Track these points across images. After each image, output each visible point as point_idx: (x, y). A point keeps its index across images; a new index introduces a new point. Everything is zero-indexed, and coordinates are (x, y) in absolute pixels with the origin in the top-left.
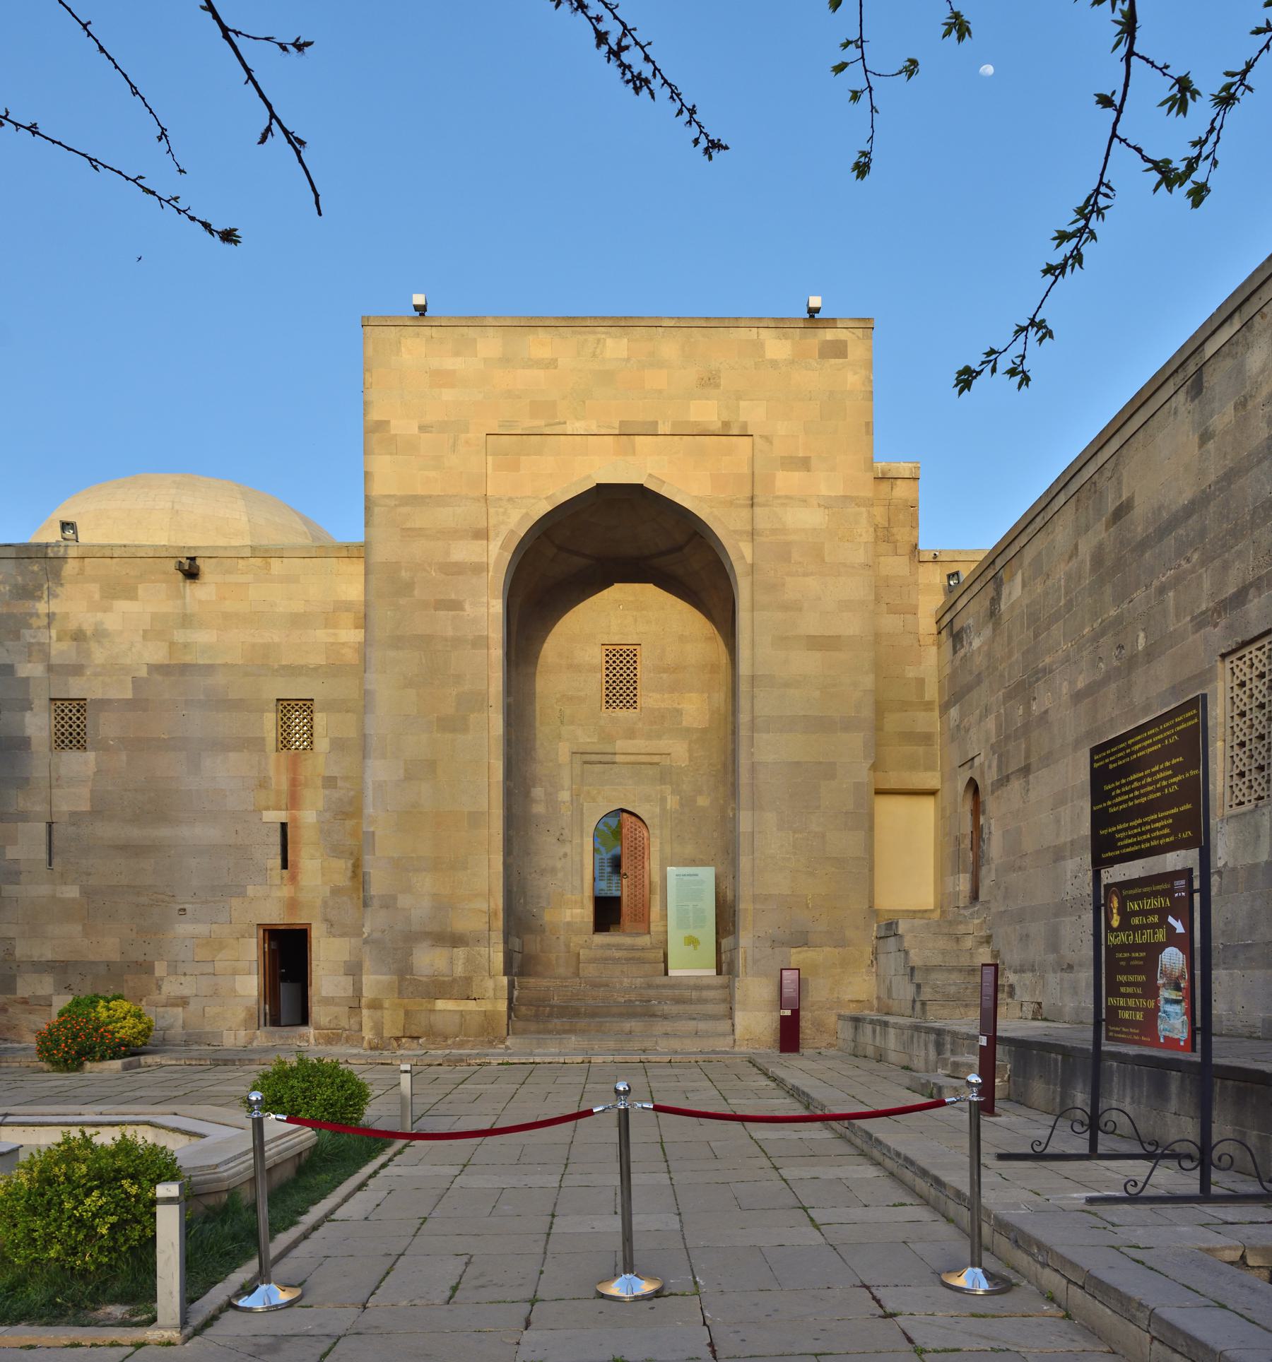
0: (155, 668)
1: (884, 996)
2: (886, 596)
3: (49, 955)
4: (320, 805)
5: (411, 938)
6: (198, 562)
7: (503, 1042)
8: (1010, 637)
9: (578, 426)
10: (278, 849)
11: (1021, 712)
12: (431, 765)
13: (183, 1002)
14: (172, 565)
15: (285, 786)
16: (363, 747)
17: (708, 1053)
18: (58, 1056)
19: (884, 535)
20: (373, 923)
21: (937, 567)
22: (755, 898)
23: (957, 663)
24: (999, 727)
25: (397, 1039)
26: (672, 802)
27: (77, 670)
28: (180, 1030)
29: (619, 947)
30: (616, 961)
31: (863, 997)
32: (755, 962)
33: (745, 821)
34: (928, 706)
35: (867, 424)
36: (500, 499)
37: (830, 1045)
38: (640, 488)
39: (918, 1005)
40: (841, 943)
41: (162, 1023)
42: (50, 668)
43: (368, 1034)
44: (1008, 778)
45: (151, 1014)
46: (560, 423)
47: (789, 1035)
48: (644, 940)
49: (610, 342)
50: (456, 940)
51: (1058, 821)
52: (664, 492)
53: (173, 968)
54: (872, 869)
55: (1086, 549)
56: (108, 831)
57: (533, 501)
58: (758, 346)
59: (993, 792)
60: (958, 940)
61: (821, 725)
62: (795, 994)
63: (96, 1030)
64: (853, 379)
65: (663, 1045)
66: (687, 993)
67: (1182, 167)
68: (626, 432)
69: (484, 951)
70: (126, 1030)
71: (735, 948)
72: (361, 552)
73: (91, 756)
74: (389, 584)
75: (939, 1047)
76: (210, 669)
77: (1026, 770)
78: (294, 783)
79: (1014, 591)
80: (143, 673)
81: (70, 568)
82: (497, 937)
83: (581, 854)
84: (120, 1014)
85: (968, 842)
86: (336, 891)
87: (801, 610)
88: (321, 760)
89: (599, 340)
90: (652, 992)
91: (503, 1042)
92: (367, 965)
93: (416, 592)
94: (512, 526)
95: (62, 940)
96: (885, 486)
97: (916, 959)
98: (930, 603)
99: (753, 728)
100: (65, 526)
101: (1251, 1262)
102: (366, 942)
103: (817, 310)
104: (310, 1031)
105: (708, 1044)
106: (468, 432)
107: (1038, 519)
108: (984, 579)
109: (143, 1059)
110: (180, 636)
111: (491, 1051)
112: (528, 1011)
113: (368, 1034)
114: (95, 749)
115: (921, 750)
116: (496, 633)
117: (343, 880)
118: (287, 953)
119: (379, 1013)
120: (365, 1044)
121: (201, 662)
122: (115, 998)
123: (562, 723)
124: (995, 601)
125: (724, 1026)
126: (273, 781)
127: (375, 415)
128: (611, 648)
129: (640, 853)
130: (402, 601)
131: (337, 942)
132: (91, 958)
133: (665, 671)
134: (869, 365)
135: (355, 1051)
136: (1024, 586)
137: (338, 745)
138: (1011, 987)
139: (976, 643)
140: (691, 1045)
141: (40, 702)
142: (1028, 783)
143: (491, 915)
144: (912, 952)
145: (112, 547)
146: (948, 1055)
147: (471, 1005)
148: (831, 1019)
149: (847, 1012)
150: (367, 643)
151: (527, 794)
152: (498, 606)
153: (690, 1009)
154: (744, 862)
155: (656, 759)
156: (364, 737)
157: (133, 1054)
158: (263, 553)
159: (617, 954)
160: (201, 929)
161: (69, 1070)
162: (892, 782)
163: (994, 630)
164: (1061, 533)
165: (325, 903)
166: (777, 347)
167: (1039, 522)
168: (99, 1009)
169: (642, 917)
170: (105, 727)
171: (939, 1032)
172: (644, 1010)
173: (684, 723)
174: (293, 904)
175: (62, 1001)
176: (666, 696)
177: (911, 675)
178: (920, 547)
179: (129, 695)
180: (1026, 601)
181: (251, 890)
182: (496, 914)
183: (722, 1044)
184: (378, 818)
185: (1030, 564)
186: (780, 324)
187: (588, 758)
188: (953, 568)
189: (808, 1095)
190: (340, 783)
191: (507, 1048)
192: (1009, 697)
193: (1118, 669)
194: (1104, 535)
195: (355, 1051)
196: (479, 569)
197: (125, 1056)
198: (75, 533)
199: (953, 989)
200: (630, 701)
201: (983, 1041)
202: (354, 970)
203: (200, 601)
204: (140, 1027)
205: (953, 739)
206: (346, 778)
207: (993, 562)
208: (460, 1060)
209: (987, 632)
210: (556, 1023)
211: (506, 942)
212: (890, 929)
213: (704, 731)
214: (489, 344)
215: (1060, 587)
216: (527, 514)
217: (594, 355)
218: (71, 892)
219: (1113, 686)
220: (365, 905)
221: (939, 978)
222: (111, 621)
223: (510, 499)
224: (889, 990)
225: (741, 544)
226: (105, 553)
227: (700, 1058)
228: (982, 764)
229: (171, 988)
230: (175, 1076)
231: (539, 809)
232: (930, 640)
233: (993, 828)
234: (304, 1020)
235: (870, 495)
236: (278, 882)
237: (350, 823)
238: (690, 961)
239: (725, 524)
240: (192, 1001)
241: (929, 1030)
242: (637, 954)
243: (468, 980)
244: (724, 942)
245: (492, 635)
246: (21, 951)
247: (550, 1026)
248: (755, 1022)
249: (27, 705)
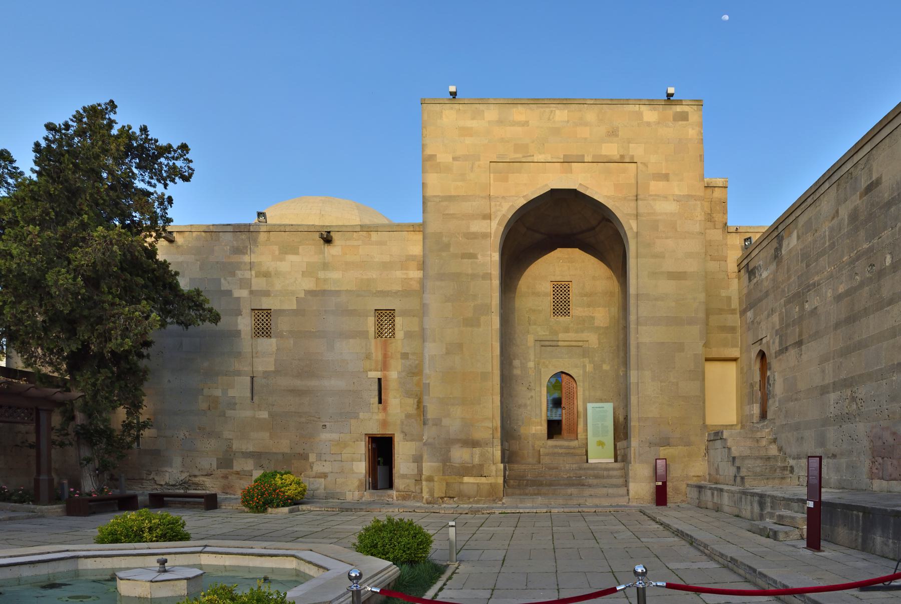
0: (309, 292)
1: (713, 472)
2: (712, 253)
3: (251, 449)
4: (399, 368)
5: (450, 442)
6: (332, 234)
7: (501, 500)
8: (788, 270)
9: (541, 158)
10: (376, 393)
11: (797, 310)
12: (460, 346)
13: (324, 476)
14: (317, 235)
15: (380, 357)
16: (422, 335)
17: (614, 507)
18: (253, 504)
19: (709, 218)
20: (429, 434)
21: (737, 235)
22: (639, 419)
23: (752, 286)
24: (781, 320)
25: (442, 498)
26: (589, 368)
27: (267, 294)
28: (323, 491)
29: (561, 447)
30: (560, 454)
31: (701, 474)
32: (640, 455)
33: (633, 376)
34: (733, 312)
35: (701, 156)
37: (683, 501)
38: (574, 191)
39: (738, 479)
40: (688, 444)
41: (312, 487)
42: (251, 292)
43: (426, 495)
44: (787, 349)
45: (307, 483)
47: (661, 496)
48: (575, 443)
49: (558, 112)
50: (475, 444)
51: (823, 371)
52: (588, 193)
53: (319, 457)
54: (704, 403)
55: (844, 213)
56: (284, 382)
58: (640, 115)
59: (776, 357)
60: (758, 441)
61: (674, 321)
62: (664, 473)
63: (275, 491)
64: (692, 133)
65: (590, 502)
66: (601, 472)
68: (567, 161)
69: (490, 450)
70: (291, 491)
71: (629, 446)
72: (420, 228)
73: (273, 340)
74: (435, 244)
75: (762, 505)
76: (337, 293)
77: (800, 343)
78: (385, 356)
79: (792, 242)
80: (302, 295)
81: (262, 237)
82: (497, 442)
83: (540, 396)
84: (288, 482)
85: (758, 386)
86: (408, 416)
87: (664, 257)
88: (399, 343)
90: (582, 472)
91: (501, 500)
92: (425, 457)
93: (451, 249)
94: (503, 213)
95: (259, 440)
96: (709, 191)
97: (735, 452)
98: (734, 255)
99: (638, 323)
100: (260, 214)
102: (425, 444)
103: (672, 95)
104: (394, 493)
105: (614, 501)
106: (479, 160)
107: (809, 200)
108: (770, 238)
109: (300, 507)
110: (321, 275)
111: (494, 505)
112: (515, 483)
113: (426, 495)
114: (276, 337)
115: (729, 336)
116: (495, 272)
117: (412, 410)
118: (381, 449)
119: (432, 484)
120: (424, 501)
121: (333, 289)
122: (286, 473)
124: (778, 249)
125: (623, 491)
126: (374, 355)
127: (429, 151)
129: (572, 396)
130: (444, 254)
131: (409, 443)
132: (274, 450)
133: (585, 295)
134: (701, 125)
135: (418, 504)
136: (798, 238)
137: (409, 335)
138: (792, 467)
139: (765, 274)
140: (605, 502)
141: (246, 311)
142: (801, 350)
143: (494, 430)
144: (733, 449)
145: (285, 225)
146: (768, 510)
147: (483, 480)
148: (683, 487)
149: (694, 482)
150: (425, 277)
151: (511, 364)
152: (496, 257)
153: (604, 481)
154: (633, 399)
155: (580, 344)
156: (423, 329)
157: (295, 504)
158: (367, 229)
159: (560, 451)
160: (335, 436)
161: (259, 512)
162: (714, 354)
163: (777, 266)
164: (826, 205)
165: (402, 423)
166: (650, 115)
167: (810, 201)
169: (573, 431)
170: (281, 324)
171: (762, 496)
172: (578, 482)
173: (596, 324)
174: (384, 423)
175: (257, 474)
177: (724, 295)
178: (728, 224)
179: (295, 307)
180: (799, 248)
181: (361, 415)
182: (496, 429)
183: (623, 501)
184: (431, 376)
185: (803, 226)
186: (651, 103)
187: (543, 343)
188: (748, 235)
189: (691, 537)
190: (410, 357)
191: (503, 504)
192: (789, 301)
193: (871, 278)
194: (858, 202)
195: (418, 504)
196: (486, 236)
197: (290, 505)
198: (265, 218)
199: (758, 470)
200: (567, 313)
201: (811, 504)
202: (418, 460)
203: (333, 256)
204: (299, 489)
205: (749, 329)
206: (414, 354)
207: (777, 228)
208: (475, 512)
209: (773, 267)
210: (530, 489)
211: (502, 445)
212: (717, 435)
213: (607, 328)
214: (491, 113)
215: (825, 236)
217: (549, 119)
218: (264, 415)
219: (867, 289)
220: (424, 424)
221: (749, 463)
222: (283, 266)
223: (503, 197)
224: (717, 470)
225: (631, 221)
226: (282, 229)
227: (611, 509)
228: (768, 342)
229: (318, 468)
230: (319, 517)
231: (517, 372)
232: (734, 275)
233: (776, 377)
234: (390, 486)
235: (702, 194)
237: (416, 379)
238: (600, 454)
239: (621, 210)
240: (329, 475)
241: (753, 495)
242: (572, 451)
243: (481, 466)
244: (618, 444)
245: (493, 272)
246: (236, 446)
247: (527, 491)
248: (641, 488)
249: (239, 313)
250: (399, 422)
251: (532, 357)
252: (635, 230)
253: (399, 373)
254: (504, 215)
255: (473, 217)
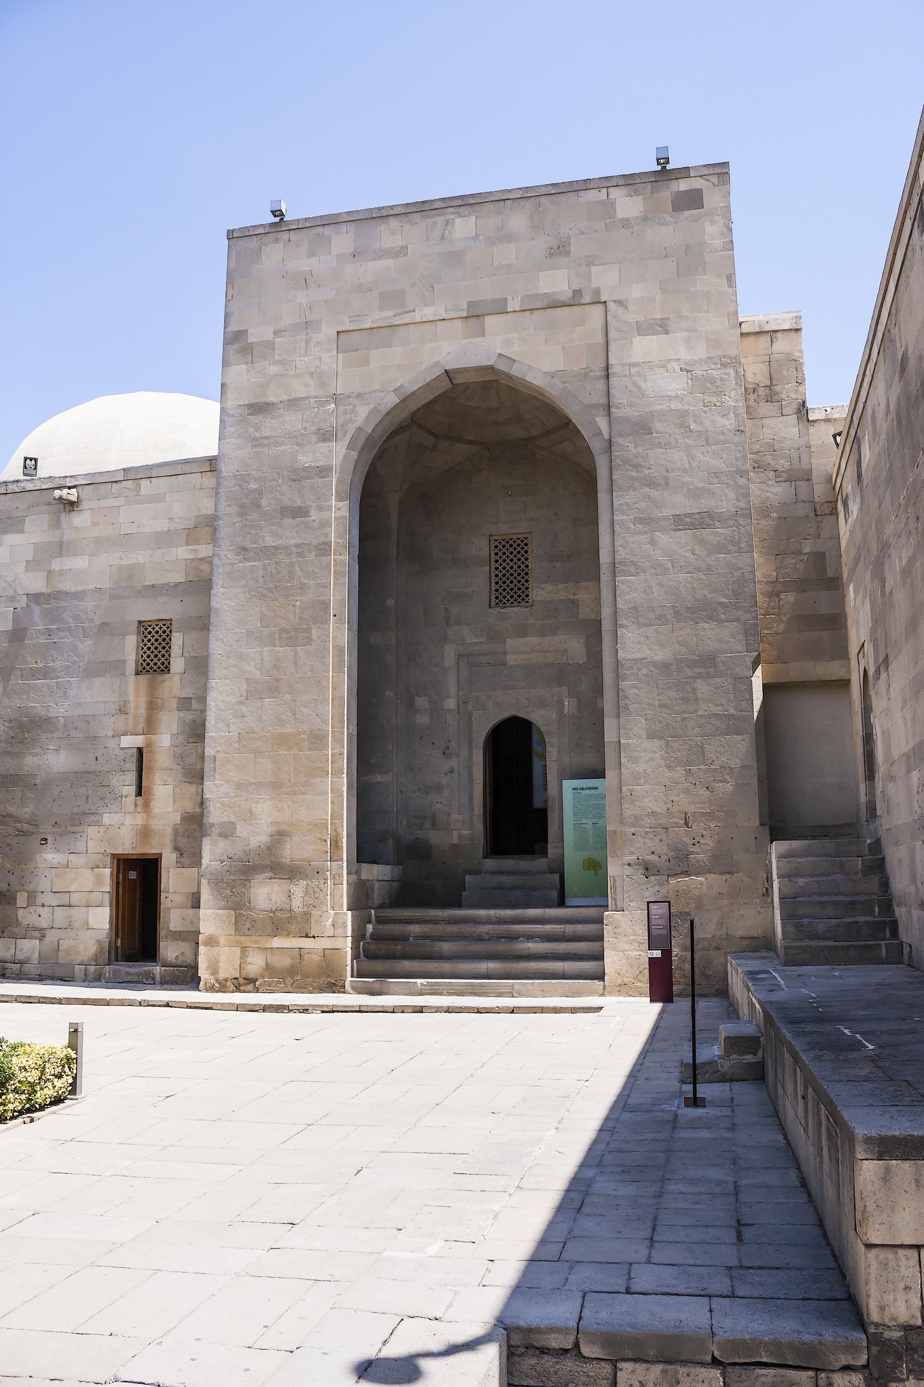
0: (36, 598)
4: (175, 727)
9: (428, 313)
15: (142, 711)
26: (569, 705)
36: (349, 397)
46: (409, 312)
49: (458, 222)
57: (383, 394)
58: (608, 207)
67: (198, 810)
76: (79, 596)
89: (447, 222)
94: (358, 424)
101: (586, 1350)
123: (447, 623)
126: (132, 705)
128: (500, 538)
168: (902, 1269)
173: (581, 616)
174: (145, 833)
176: (560, 586)
178: (808, 405)
196: (324, 471)
216: (375, 408)
223: (359, 396)
236: (131, 807)
250: (169, 831)
251: (452, 688)
252: (606, 436)
253: (173, 736)
254: (359, 429)
255: (298, 440)
